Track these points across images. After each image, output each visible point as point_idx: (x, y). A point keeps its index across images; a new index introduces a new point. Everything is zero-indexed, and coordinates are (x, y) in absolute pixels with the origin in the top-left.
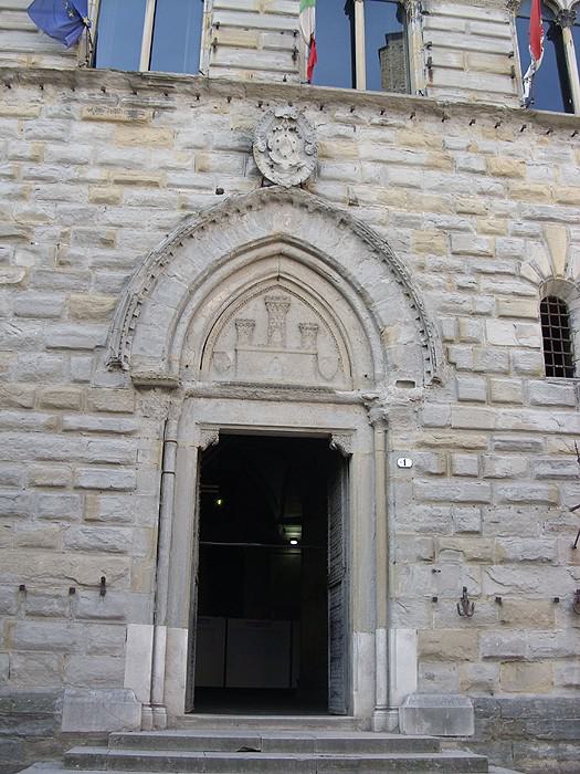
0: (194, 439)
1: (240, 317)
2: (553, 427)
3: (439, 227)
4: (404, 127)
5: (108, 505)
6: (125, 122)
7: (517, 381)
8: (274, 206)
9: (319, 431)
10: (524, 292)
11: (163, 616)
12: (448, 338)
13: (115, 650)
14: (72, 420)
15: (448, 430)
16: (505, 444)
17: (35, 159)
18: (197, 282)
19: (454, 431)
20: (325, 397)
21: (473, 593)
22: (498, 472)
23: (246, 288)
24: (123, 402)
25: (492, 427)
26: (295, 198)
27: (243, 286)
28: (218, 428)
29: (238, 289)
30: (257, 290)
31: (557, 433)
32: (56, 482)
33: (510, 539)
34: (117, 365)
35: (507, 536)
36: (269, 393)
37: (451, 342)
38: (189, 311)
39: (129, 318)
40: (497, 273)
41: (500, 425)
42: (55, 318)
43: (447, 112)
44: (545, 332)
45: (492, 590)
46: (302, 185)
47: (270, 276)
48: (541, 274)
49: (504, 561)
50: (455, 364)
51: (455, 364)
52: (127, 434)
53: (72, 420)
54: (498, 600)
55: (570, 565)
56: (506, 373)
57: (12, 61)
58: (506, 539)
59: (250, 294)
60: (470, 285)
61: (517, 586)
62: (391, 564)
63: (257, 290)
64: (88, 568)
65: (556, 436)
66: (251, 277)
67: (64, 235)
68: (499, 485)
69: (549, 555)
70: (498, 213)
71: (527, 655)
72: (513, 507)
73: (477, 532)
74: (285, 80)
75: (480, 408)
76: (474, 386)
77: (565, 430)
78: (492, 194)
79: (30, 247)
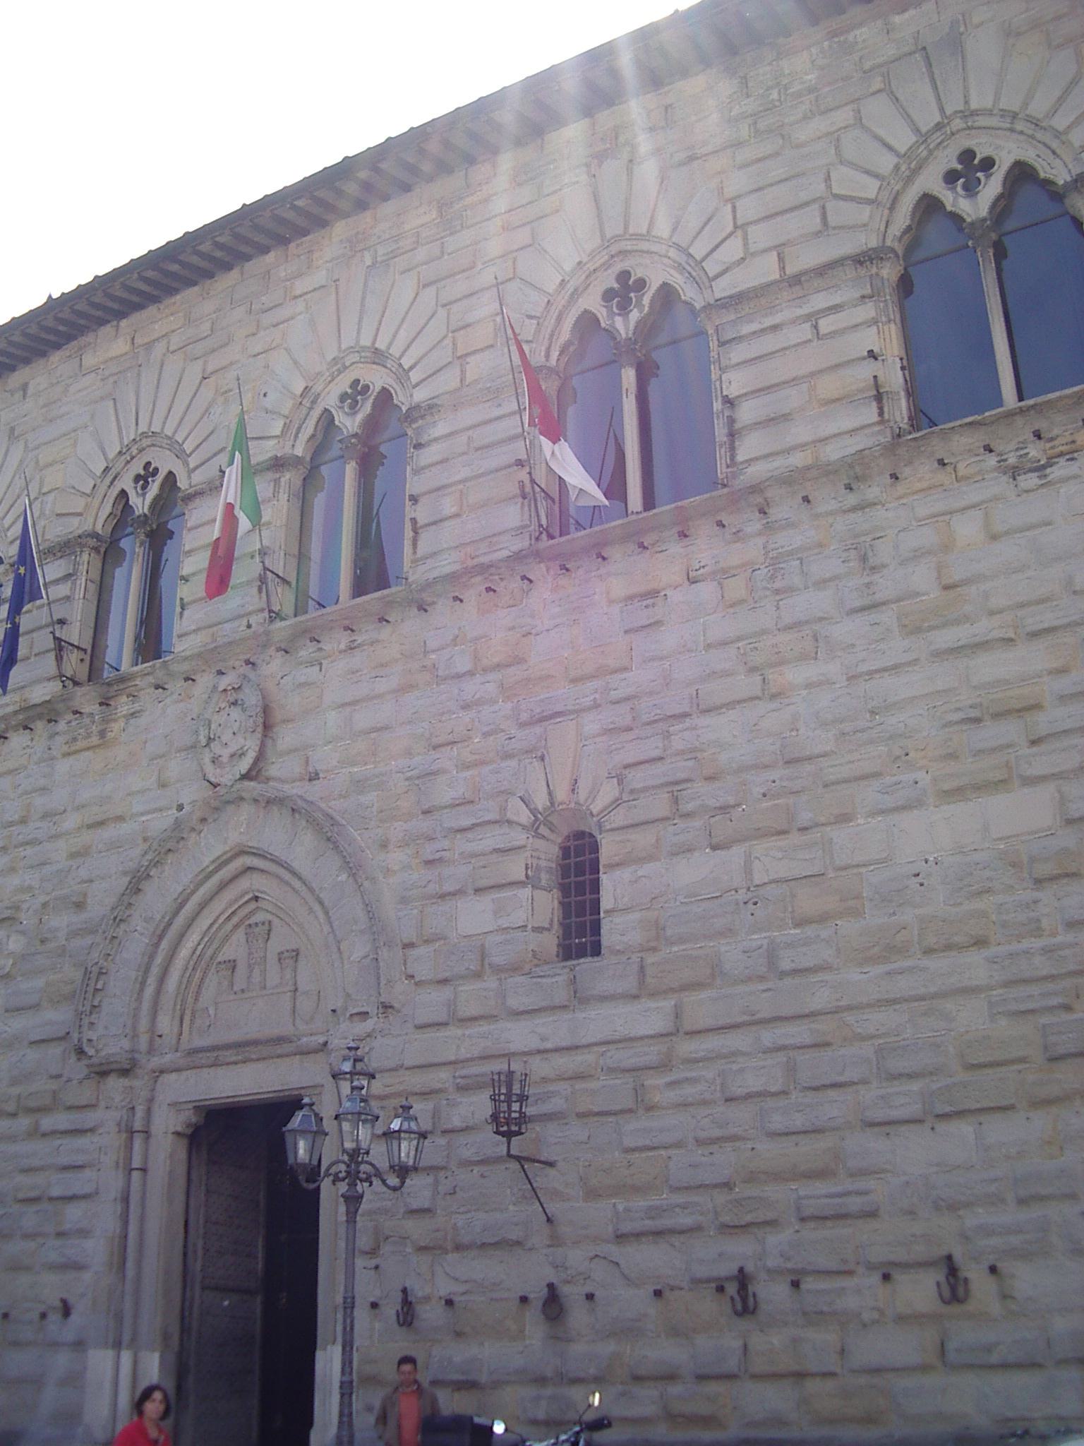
0: (168, 1124)
1: (219, 959)
2: (535, 1043)
3: (407, 779)
4: (378, 641)
5: (74, 1214)
6: (98, 746)
7: (491, 983)
8: (231, 808)
9: (213, 1102)
10: (509, 845)
11: (126, 1337)
12: (406, 941)
13: (74, 1379)
14: (47, 1123)
15: (401, 1072)
16: (469, 1081)
17: (23, 821)
18: (159, 932)
19: (408, 1073)
20: (287, 1048)
21: (420, 1294)
22: (457, 1122)
23: (220, 921)
24: (85, 1094)
25: (453, 1058)
26: (244, 794)
27: (215, 921)
28: (190, 1106)
29: (212, 925)
30: (235, 920)
31: (539, 1052)
32: (32, 1194)
33: (469, 1215)
34: (80, 1052)
35: (469, 1211)
36: (230, 1055)
37: (410, 945)
38: (155, 970)
39: (89, 996)
40: (474, 826)
41: (464, 1053)
42: (35, 1007)
43: (426, 597)
44: (565, 906)
45: (445, 1288)
46: (246, 777)
47: (246, 898)
48: (534, 812)
49: (458, 1248)
50: (413, 977)
51: (413, 977)
52: (92, 1130)
53: (47, 1123)
54: (449, 1303)
55: (549, 1246)
56: (478, 975)
57: (7, 705)
58: (463, 1217)
59: (229, 926)
60: (437, 856)
61: (475, 1281)
62: (1015, 1067)
63: (235, 920)
64: (51, 1287)
65: (538, 1057)
66: (223, 906)
67: (45, 905)
68: (461, 1139)
69: (514, 1234)
70: (486, 729)
71: (483, 1378)
72: (476, 1169)
73: (428, 1211)
74: (249, 626)
75: (443, 1033)
76: (431, 1003)
77: (549, 1045)
78: (479, 703)
79: (21, 928)
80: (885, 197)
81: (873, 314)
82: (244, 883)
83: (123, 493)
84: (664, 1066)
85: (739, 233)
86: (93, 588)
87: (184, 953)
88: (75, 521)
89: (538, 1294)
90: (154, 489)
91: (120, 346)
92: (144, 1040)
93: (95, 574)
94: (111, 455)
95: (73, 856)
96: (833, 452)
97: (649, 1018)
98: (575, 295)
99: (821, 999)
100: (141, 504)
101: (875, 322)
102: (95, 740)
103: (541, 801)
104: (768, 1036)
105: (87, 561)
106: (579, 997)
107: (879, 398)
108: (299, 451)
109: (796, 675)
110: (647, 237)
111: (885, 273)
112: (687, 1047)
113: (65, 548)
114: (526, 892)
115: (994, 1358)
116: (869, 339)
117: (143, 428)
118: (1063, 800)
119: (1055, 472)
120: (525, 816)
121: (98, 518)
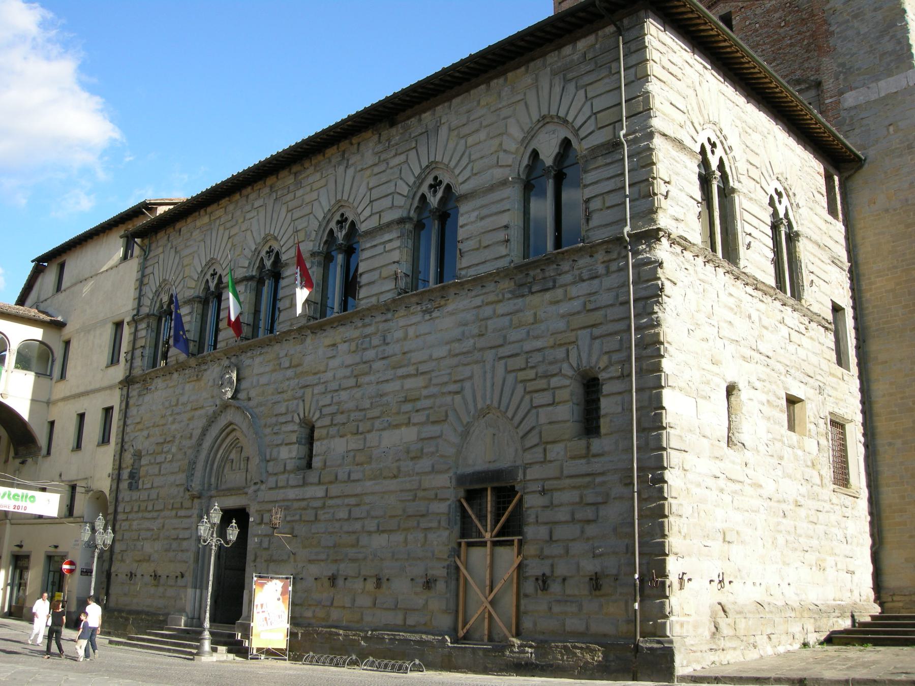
5: (185, 544)
11: (198, 584)
80: (411, 194)
81: (399, 244)
82: (234, 434)
83: (331, 231)
84: (323, 507)
85: (593, 117)
86: (199, 317)
87: (219, 456)
88: (192, 291)
89: (385, 585)
90: (440, 194)
91: (206, 219)
92: (206, 486)
93: (200, 311)
94: (320, 219)
95: (189, 419)
96: (383, 298)
97: (319, 492)
98: (419, 187)
99: (359, 490)
100: (340, 235)
101: (399, 247)
102: (195, 378)
103: (302, 416)
104: (347, 501)
105: (197, 307)
106: (305, 484)
107: (396, 279)
108: (254, 274)
109: (366, 379)
110: (441, 163)
111: (407, 226)
112: (330, 502)
113: (189, 301)
114: (297, 446)
115: (385, 606)
116: (396, 255)
117: (267, 232)
118: (419, 433)
119: (434, 315)
120: (297, 420)
121: (199, 291)
